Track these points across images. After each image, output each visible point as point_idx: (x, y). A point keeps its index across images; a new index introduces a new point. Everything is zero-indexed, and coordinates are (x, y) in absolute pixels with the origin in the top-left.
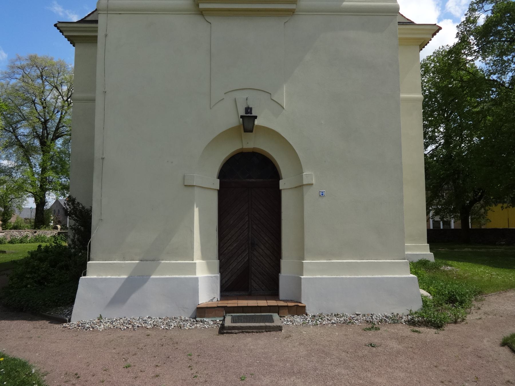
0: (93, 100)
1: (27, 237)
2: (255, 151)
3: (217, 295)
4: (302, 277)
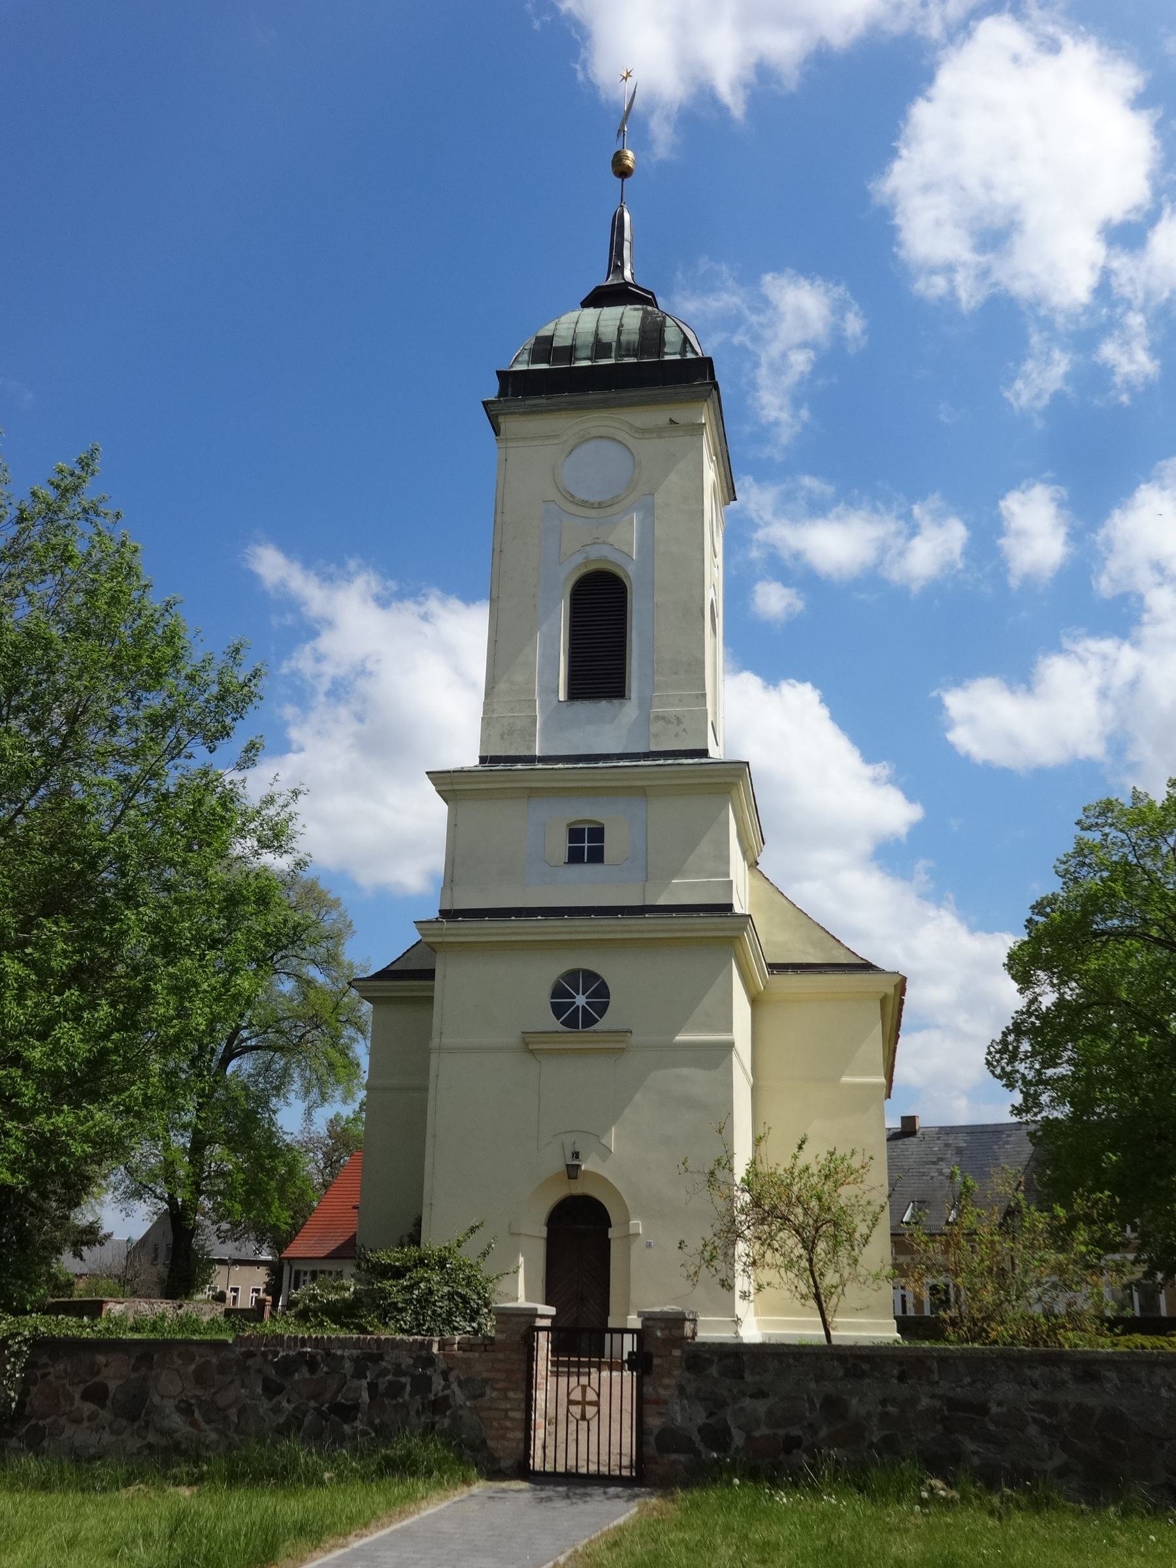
0: (426, 1089)
1: (163, 1317)
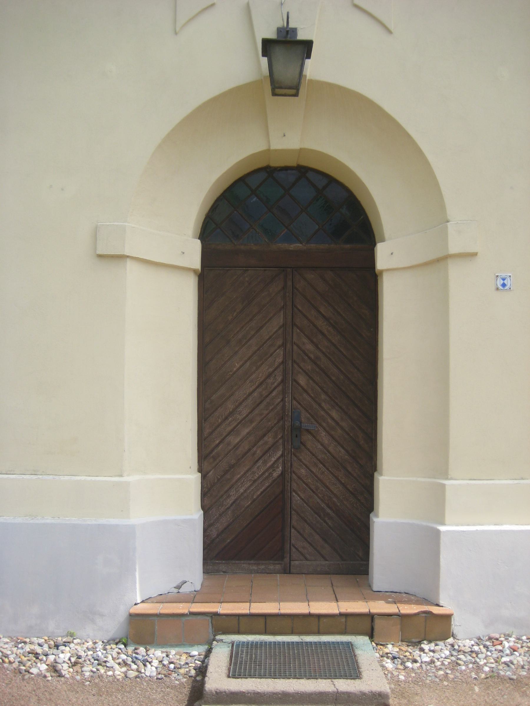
2: (304, 163)
3: (193, 574)
4: (442, 528)
